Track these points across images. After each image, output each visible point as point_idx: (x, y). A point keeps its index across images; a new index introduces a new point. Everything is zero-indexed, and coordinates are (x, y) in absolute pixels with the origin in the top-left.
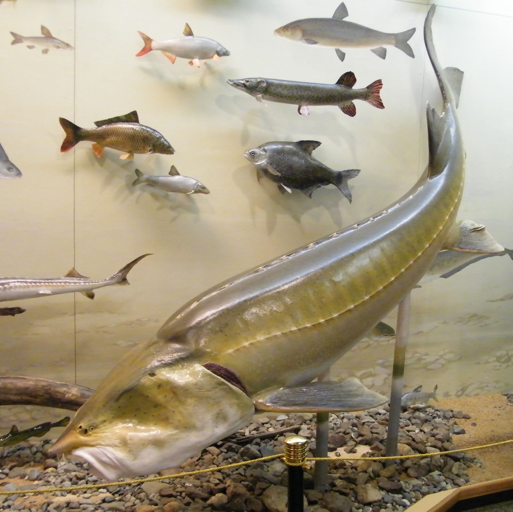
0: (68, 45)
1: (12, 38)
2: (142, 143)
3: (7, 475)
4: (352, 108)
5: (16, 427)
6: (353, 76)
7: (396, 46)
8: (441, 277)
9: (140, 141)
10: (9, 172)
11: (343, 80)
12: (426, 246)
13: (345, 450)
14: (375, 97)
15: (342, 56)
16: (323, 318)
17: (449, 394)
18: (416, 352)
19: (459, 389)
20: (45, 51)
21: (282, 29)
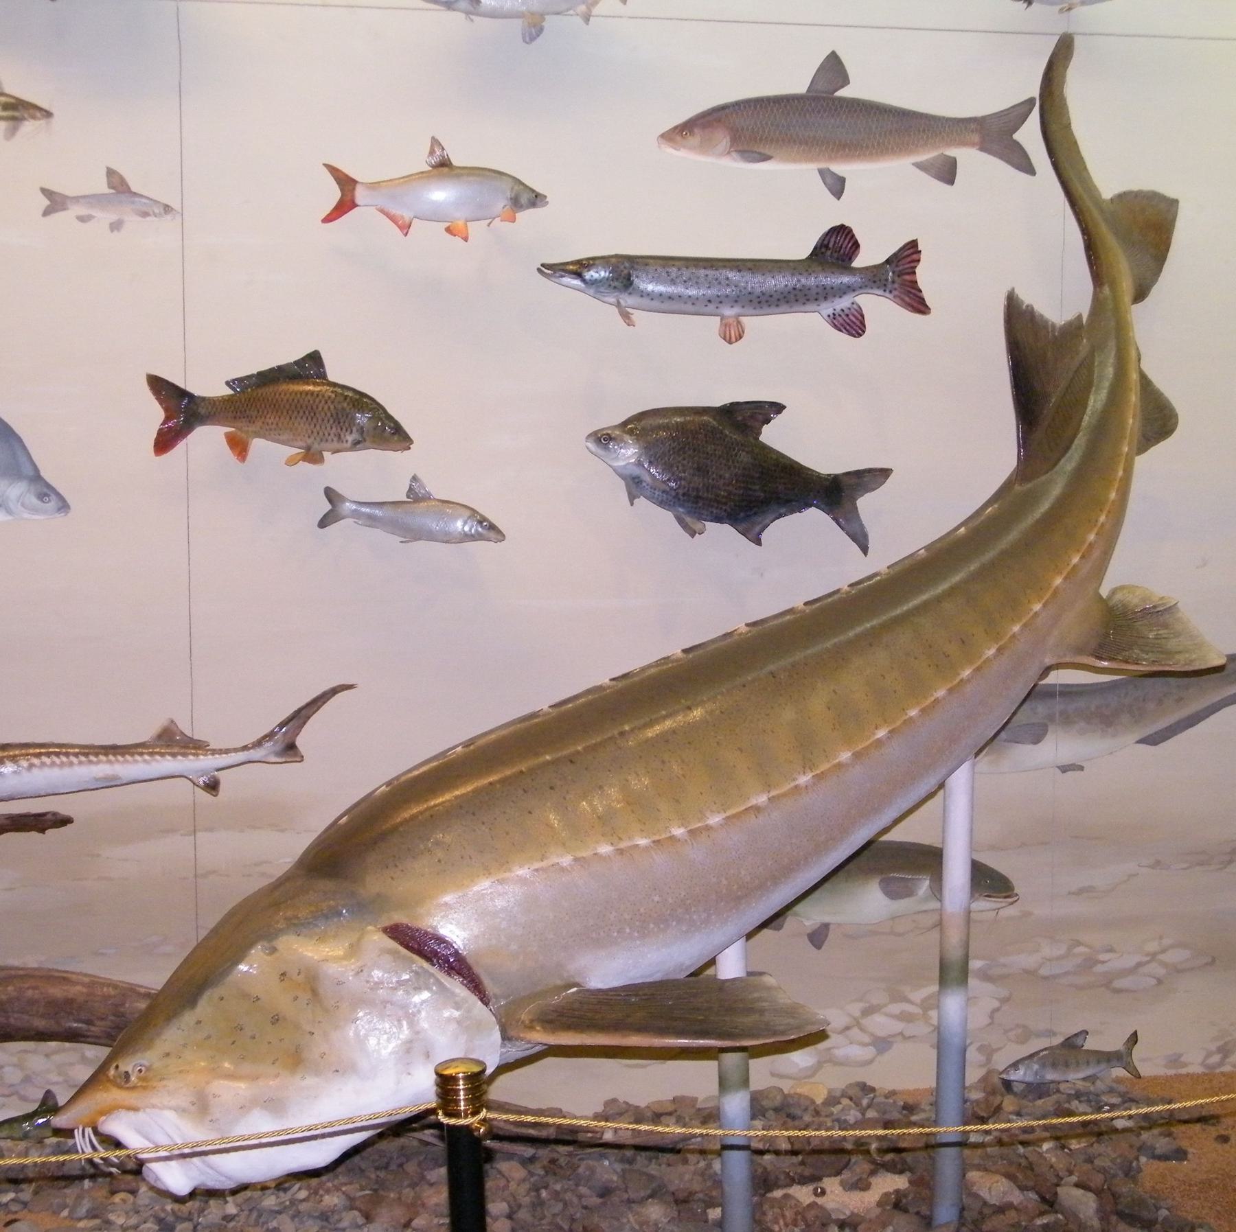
0: (167, 209)
1: (46, 202)
2: (334, 426)
3: (25, 1204)
4: (854, 316)
5: (54, 1097)
6: (849, 237)
7: (983, 149)
8: (1140, 742)
9: (328, 421)
10: (39, 502)
11: (827, 247)
12: (987, 651)
13: (842, 1183)
14: (907, 283)
15: (837, 187)
16: (683, 825)
17: (1182, 1059)
18: (1078, 943)
19: (1213, 1047)
20: (116, 226)
21: (678, 130)
